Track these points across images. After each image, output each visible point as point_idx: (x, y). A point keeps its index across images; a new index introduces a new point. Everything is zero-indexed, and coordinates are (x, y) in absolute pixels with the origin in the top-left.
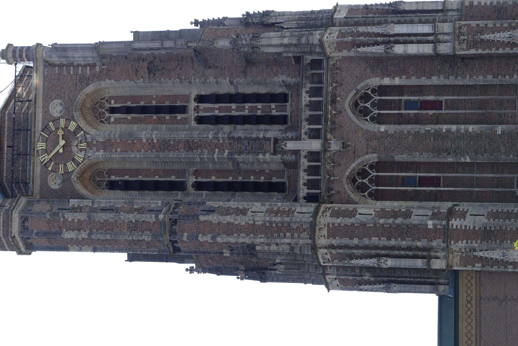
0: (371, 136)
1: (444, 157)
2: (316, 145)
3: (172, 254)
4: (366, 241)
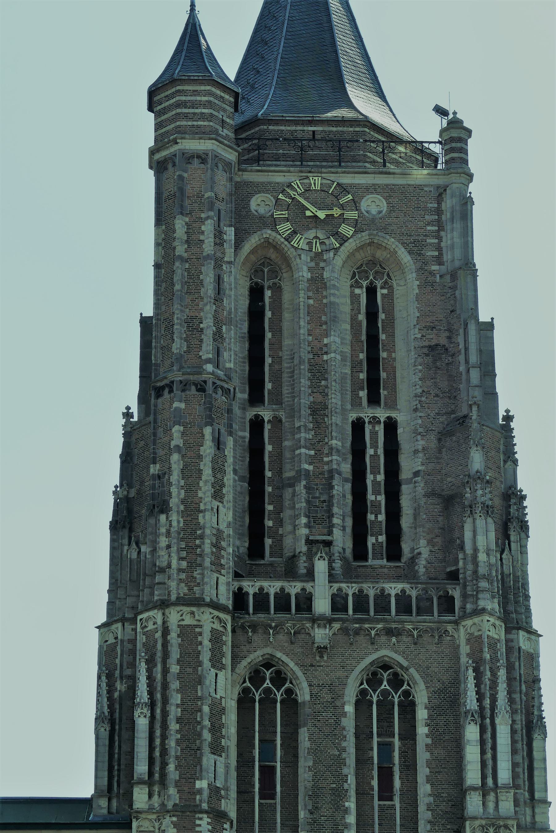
0: (336, 690)
1: (305, 806)
2: (322, 605)
3: (152, 385)
4: (175, 685)
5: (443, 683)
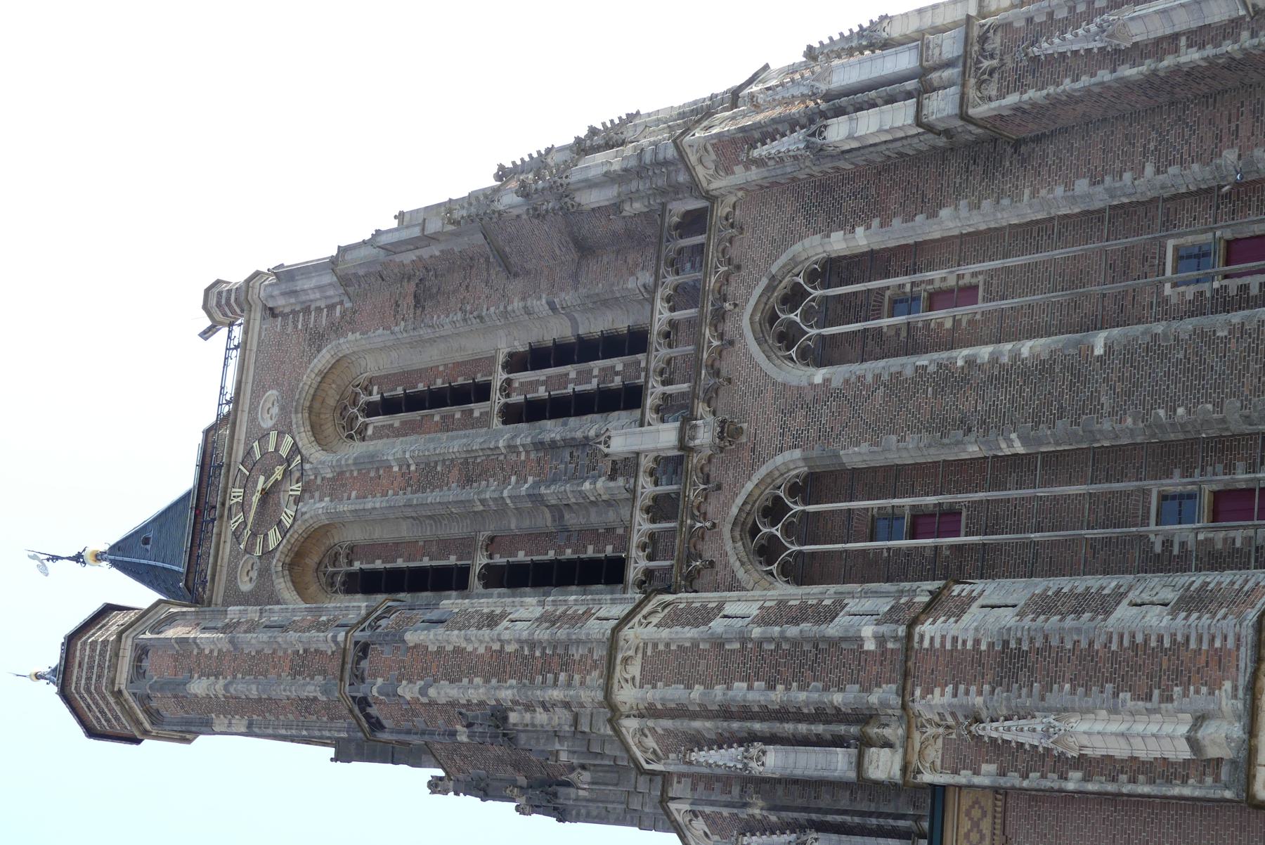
1: (958, 443)
2: (664, 436)
5: (798, 211)
